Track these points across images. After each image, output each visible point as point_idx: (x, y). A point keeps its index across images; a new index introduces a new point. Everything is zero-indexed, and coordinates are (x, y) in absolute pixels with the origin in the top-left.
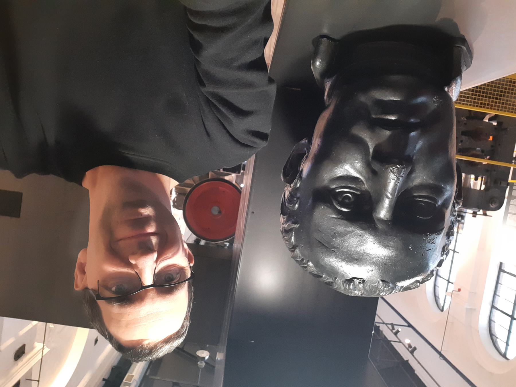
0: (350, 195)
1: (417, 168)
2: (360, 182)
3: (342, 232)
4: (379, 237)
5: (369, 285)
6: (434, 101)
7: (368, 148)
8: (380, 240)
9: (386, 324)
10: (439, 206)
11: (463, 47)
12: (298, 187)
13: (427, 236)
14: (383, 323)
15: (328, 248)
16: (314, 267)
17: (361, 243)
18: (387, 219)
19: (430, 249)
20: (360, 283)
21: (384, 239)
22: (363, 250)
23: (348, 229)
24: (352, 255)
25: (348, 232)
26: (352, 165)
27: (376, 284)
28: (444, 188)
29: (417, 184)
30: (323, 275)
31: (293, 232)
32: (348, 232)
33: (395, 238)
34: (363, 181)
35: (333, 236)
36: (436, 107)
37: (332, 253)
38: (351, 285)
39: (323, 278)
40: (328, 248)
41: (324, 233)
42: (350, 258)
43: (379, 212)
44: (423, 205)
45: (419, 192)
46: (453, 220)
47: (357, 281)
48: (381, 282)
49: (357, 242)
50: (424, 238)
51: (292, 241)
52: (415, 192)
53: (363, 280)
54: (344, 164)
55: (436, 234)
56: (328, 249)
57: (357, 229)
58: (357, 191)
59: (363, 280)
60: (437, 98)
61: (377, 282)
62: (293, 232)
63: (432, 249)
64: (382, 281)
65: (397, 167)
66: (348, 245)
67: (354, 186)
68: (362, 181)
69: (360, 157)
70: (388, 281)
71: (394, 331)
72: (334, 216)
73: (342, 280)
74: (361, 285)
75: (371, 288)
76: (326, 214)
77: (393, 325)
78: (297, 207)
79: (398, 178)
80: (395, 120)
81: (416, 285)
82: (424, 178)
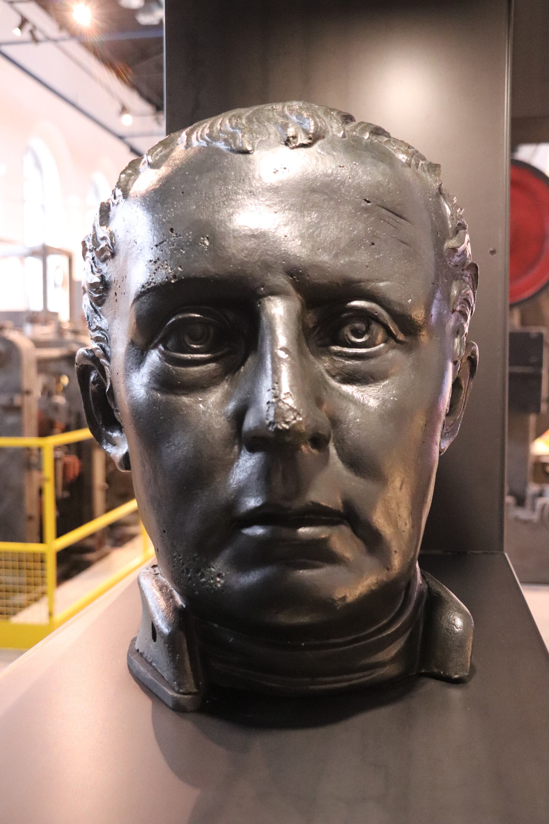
0: (354, 339)
1: (189, 417)
2: (338, 374)
3: (357, 250)
4: (279, 254)
5: (272, 136)
6: (219, 575)
7: (340, 455)
8: (277, 247)
9: (48, 39)
10: (155, 347)
11: (176, 695)
12: (456, 337)
13: (175, 277)
14: (55, 41)
15: (379, 206)
16: (393, 152)
17: (313, 232)
18: (269, 300)
19: (156, 246)
20: (294, 137)
21: (269, 253)
22: (304, 216)
23: (347, 259)
24: (325, 200)
25: (344, 252)
26: (364, 411)
27: (257, 141)
28: (154, 389)
29: (215, 390)
30: (368, 138)
31: (450, 226)
32: (344, 252)
33: (246, 259)
34: (330, 378)
35: (375, 236)
36: (212, 564)
37: (369, 197)
38: (312, 128)
39: (366, 131)
40: (379, 206)
41: (393, 239)
42: (329, 193)
43: (288, 311)
44: (194, 344)
45: (205, 372)
46: (96, 318)
47: (302, 139)
48: (249, 148)
49: (321, 231)
50: (180, 269)
51: (448, 205)
52: (215, 370)
53: (290, 146)
54: (382, 410)
55: (152, 285)
56: (379, 202)
57: (330, 264)
58: (340, 352)
59: (290, 146)
60: (214, 583)
61: (256, 146)
62: (450, 226)
63: (152, 248)
64: (247, 152)
65: (287, 423)
66: (338, 221)
67: (347, 362)
68: (333, 377)
69: (354, 433)
70: (231, 153)
71: (28, 27)
72: (381, 284)
73: (331, 134)
74: (291, 132)
75: (265, 131)
76: (399, 286)
77: (35, 40)
78: (453, 290)
79: (277, 399)
80: (300, 527)
81: (153, 155)
82: (203, 405)
